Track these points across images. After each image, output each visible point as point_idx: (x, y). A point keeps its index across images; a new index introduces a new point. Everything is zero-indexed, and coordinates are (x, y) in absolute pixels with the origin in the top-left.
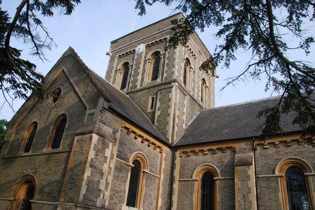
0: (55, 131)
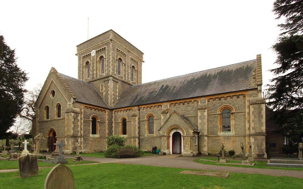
0: (57, 110)
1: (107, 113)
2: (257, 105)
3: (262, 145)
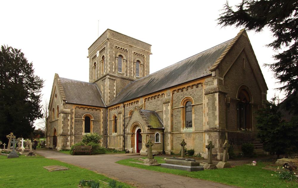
1: (102, 112)
2: (210, 95)
3: (216, 143)
